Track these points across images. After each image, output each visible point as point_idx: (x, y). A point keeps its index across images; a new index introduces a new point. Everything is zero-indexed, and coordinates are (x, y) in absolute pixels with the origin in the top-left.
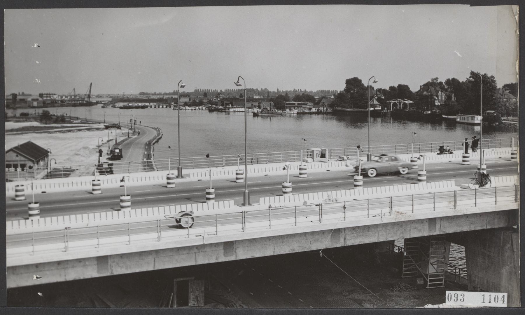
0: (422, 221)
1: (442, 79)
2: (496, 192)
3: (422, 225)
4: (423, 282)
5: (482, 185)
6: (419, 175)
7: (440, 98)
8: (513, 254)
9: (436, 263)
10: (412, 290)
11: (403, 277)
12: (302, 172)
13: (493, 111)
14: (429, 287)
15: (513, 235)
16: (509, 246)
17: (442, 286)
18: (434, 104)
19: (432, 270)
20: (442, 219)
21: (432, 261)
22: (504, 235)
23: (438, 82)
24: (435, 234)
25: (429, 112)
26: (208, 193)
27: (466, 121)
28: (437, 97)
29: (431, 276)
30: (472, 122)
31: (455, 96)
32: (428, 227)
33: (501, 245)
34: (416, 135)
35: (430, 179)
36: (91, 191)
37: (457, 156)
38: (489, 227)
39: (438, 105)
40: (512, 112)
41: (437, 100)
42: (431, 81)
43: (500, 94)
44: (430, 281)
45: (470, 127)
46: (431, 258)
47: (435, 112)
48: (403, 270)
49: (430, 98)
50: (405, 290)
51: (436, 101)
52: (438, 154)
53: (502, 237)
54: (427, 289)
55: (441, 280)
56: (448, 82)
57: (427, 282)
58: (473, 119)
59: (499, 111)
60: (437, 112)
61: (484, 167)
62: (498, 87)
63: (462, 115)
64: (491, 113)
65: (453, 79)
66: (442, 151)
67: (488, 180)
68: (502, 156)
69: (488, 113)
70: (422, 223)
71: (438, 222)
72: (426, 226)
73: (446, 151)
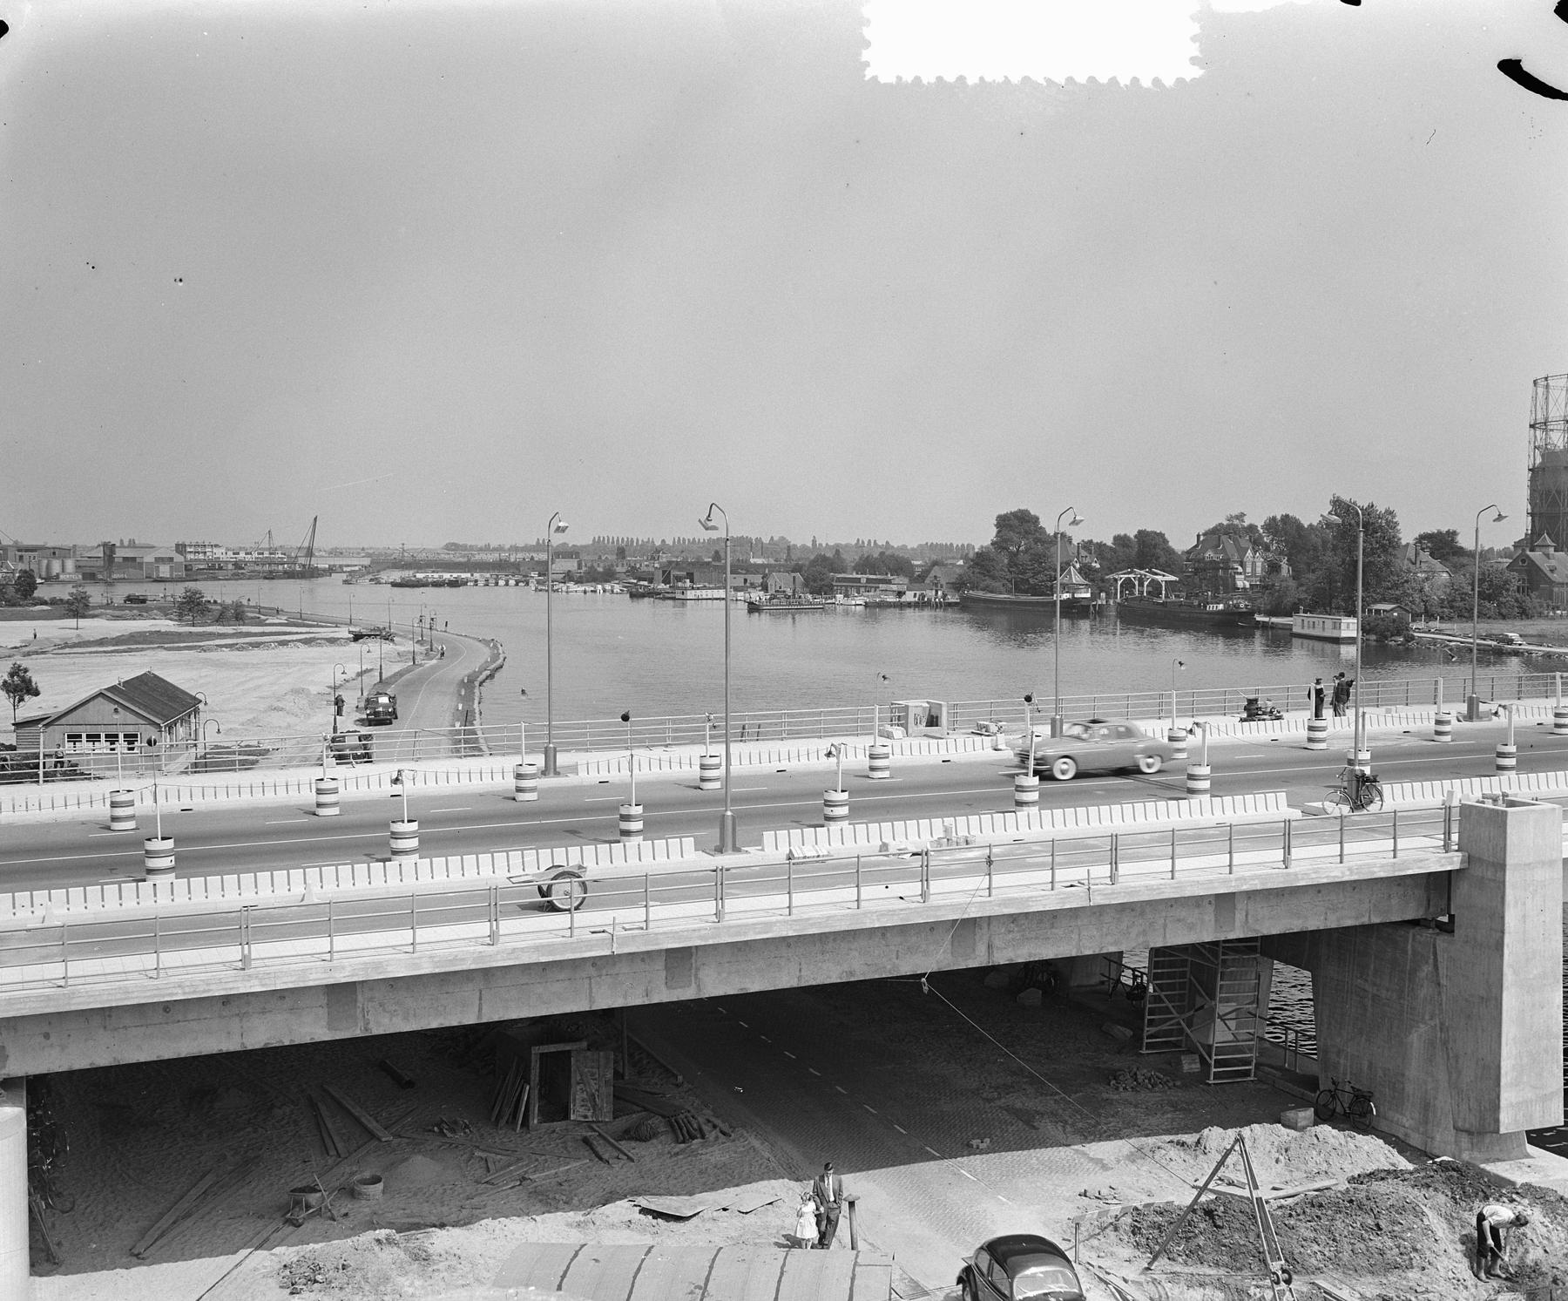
0: (1197, 901)
1: (1257, 519)
2: (1395, 825)
3: (1197, 911)
4: (1198, 1066)
5: (1358, 805)
6: (1191, 777)
7: (1249, 570)
8: (1439, 993)
9: (1233, 1015)
10: (1170, 1088)
11: (1144, 1051)
12: (878, 763)
13: (1388, 607)
14: (1214, 1079)
15: (1438, 942)
16: (1427, 969)
17: (1249, 1079)
18: (1235, 584)
19: (1221, 1034)
20: (1251, 895)
21: (1222, 1009)
22: (1414, 940)
23: (1246, 524)
24: (1232, 936)
25: (1221, 607)
26: (1501, 755)
27: (1317, 632)
28: (1242, 564)
29: (1220, 1051)
30: (1335, 634)
31: (1290, 562)
32: (1212, 917)
33: (1408, 967)
34: (1183, 668)
35: (1220, 787)
36: (698, 783)
37: (1293, 727)
38: (1376, 920)
39: (1244, 588)
40: (1439, 610)
41: (1241, 574)
42: (1225, 523)
43: (1409, 560)
44: (1218, 1063)
45: (1328, 647)
46: (1220, 1002)
47: (1237, 606)
48: (1145, 1035)
49: (1222, 568)
50: (1150, 1086)
51: (1237, 576)
52: (1242, 720)
53: (1409, 947)
54: (1210, 1085)
55: (1247, 1062)
56: (1271, 525)
57: (1210, 1065)
58: (1337, 626)
59: (1406, 605)
60: (1242, 606)
61: (1365, 756)
62: (1404, 542)
63: (1309, 615)
64: (1384, 611)
65: (1286, 518)
66: (1253, 711)
67: (1374, 793)
68: (1412, 727)
69: (1378, 611)
70: (1198, 906)
71: (1241, 906)
72: (1209, 915)
73: (1264, 713)
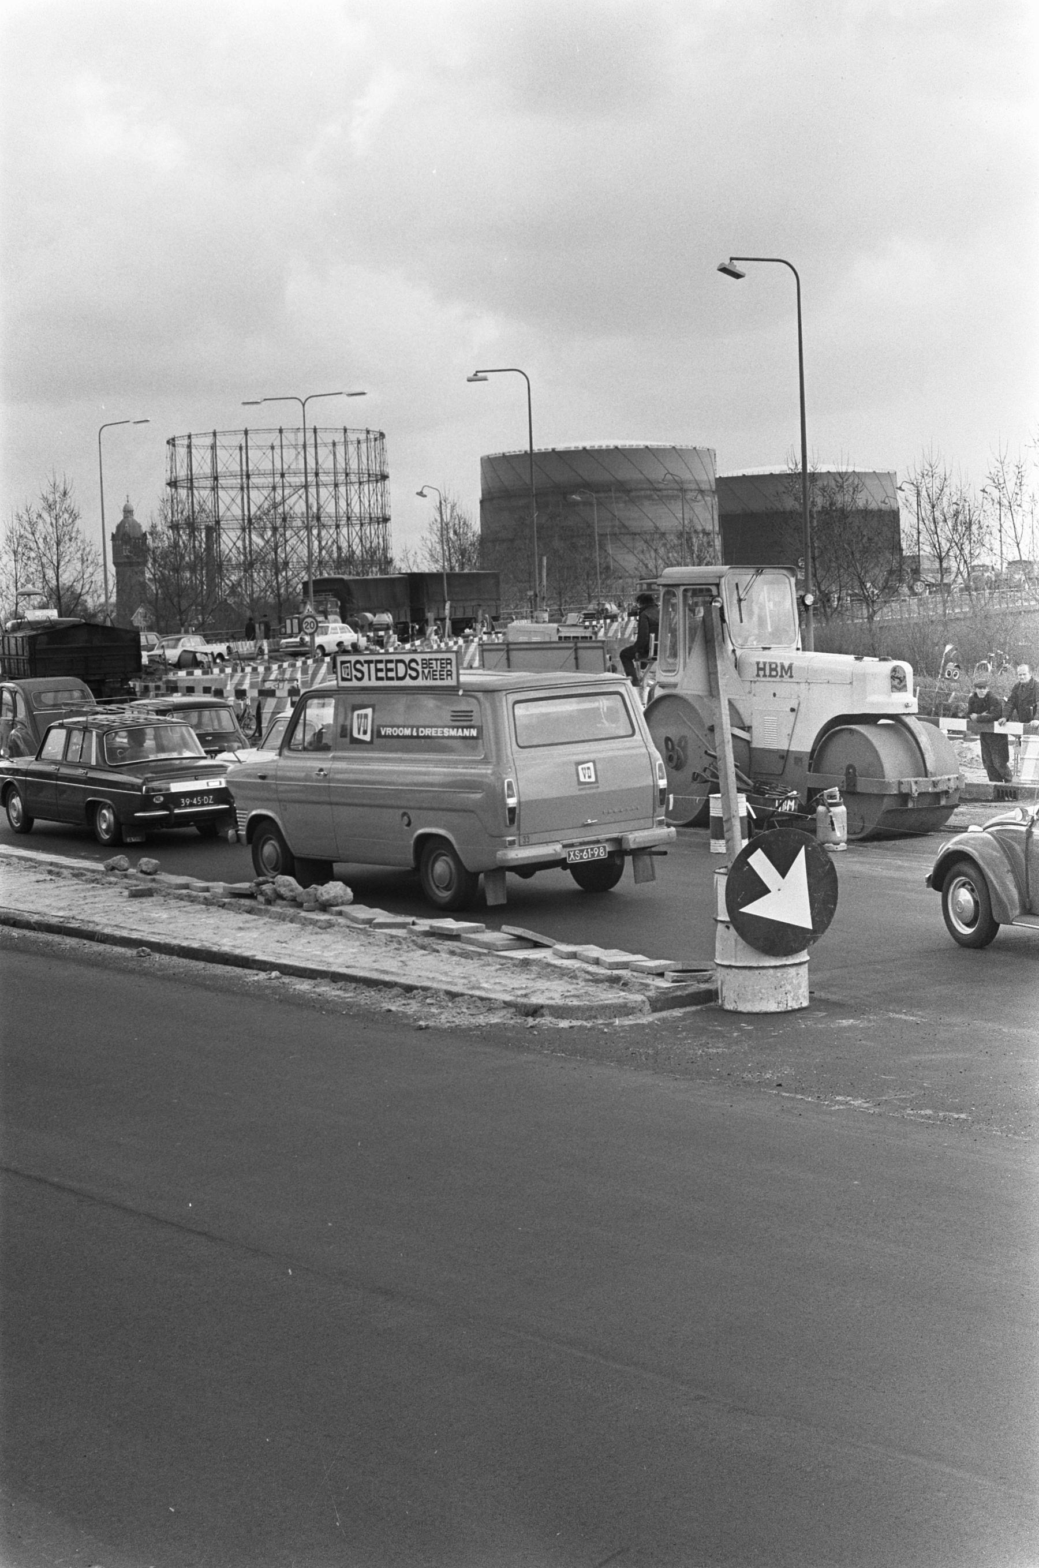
58: (55, 698)
